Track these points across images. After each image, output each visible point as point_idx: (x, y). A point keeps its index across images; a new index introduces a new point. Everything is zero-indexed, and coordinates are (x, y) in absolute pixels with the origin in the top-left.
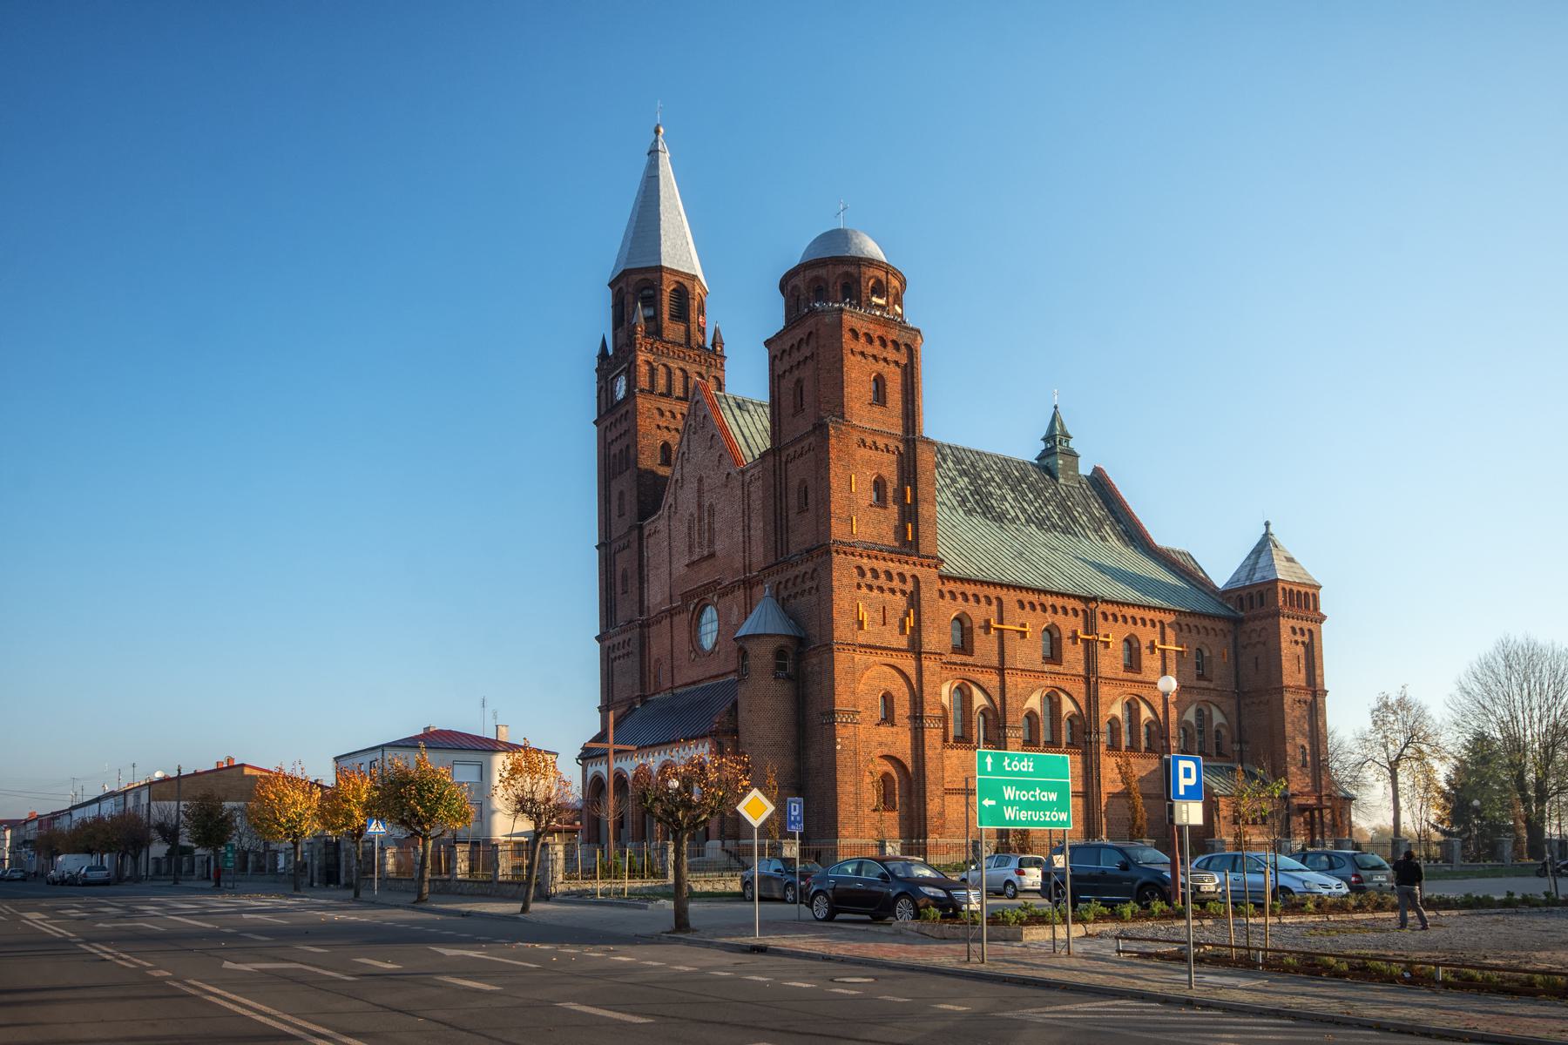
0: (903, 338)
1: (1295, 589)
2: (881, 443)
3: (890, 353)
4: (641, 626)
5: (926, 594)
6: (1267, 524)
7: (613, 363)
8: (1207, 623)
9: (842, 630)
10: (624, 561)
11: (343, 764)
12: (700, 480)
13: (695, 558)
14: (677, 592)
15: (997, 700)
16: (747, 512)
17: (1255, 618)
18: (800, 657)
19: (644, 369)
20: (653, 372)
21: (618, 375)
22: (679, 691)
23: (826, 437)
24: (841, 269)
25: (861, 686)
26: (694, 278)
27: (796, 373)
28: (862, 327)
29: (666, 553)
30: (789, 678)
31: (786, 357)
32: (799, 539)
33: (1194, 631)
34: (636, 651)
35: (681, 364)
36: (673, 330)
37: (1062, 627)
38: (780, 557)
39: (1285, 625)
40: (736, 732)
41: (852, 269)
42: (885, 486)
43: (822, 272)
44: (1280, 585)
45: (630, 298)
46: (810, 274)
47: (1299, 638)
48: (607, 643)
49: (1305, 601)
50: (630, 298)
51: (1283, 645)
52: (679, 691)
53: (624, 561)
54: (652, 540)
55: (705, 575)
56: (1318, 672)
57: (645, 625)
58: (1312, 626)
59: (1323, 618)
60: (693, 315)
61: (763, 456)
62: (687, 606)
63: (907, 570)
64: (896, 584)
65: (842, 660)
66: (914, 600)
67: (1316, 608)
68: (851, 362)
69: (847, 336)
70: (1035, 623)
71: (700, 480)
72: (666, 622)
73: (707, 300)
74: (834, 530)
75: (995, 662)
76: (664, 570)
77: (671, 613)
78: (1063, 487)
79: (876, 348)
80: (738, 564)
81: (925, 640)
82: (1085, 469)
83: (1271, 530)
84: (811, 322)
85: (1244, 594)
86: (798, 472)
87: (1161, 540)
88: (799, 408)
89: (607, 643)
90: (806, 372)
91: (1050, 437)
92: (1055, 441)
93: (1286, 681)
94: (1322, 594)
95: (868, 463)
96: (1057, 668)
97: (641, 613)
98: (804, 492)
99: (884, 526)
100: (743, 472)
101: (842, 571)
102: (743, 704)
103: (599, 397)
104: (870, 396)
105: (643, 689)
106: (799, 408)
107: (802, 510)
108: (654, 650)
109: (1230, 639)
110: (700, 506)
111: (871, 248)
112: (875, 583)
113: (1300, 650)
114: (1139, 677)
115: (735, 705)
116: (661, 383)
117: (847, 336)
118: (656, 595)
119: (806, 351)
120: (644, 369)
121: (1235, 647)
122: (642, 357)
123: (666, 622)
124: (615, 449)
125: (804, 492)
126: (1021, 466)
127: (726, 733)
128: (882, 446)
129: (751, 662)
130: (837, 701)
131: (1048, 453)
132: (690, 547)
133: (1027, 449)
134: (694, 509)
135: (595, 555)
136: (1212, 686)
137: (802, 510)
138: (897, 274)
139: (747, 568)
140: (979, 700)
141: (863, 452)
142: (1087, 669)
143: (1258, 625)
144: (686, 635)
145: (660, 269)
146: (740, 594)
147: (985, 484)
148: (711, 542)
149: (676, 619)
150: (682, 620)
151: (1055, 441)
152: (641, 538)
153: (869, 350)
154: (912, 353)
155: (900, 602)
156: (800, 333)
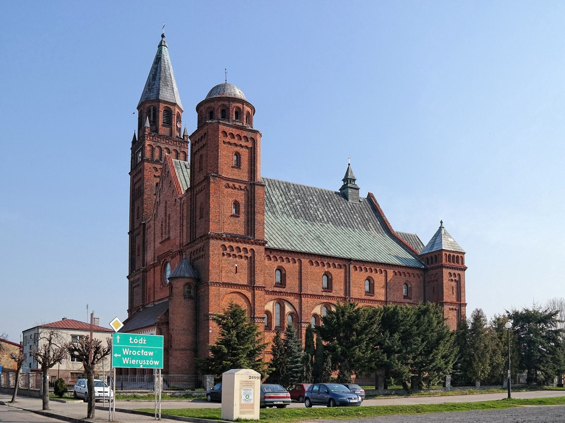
0: (250, 135)
1: (456, 255)
2: (237, 185)
3: (243, 143)
4: (143, 272)
5: (257, 258)
6: (441, 222)
7: (137, 145)
8: (409, 271)
9: (213, 277)
10: (139, 240)
11: (27, 334)
12: (166, 203)
13: (163, 239)
14: (156, 255)
15: (298, 309)
16: (182, 218)
17: (433, 268)
18: (197, 288)
19: (148, 148)
20: (153, 150)
21: (139, 151)
22: (156, 303)
23: (209, 183)
24: (221, 103)
25: (223, 302)
26: (175, 104)
27: (200, 152)
28: (229, 130)
29: (153, 237)
30: (191, 298)
31: (197, 144)
32: (199, 232)
33: (403, 275)
34: (141, 284)
35: (167, 146)
36: (163, 131)
37: (333, 273)
38: (193, 240)
39: (446, 272)
40: (168, 323)
41: (226, 103)
42: (239, 206)
43: (212, 104)
44: (444, 253)
45: (145, 114)
46: (207, 105)
47: (453, 278)
48: (132, 279)
49: (457, 260)
50: (145, 114)
51: (444, 281)
52: (156, 303)
53: (139, 240)
54: (149, 230)
55: (166, 248)
56: (462, 294)
57: (145, 271)
58: (460, 272)
59: (465, 269)
60: (174, 121)
61: (187, 191)
62: (160, 262)
63: (249, 247)
64: (242, 253)
65: (213, 290)
66: (252, 261)
67: (463, 263)
68: (222, 146)
69: (221, 134)
70: (320, 270)
71: (166, 203)
72: (152, 270)
73: (183, 116)
74: (211, 227)
75: (297, 290)
76: (152, 245)
77: (154, 266)
78: (352, 203)
79: (236, 141)
80: (178, 243)
81: (257, 280)
82: (363, 195)
83: (443, 225)
84: (206, 128)
85: (429, 256)
86: (200, 198)
87: (397, 227)
88: (201, 169)
89: (132, 279)
90: (203, 152)
91: (346, 179)
92: (348, 181)
93: (446, 299)
94: (466, 257)
95: (230, 195)
96: (329, 294)
97: (143, 266)
98: (202, 209)
99: (238, 225)
100: (181, 199)
101: (215, 246)
102: (170, 311)
103: (131, 161)
104: (234, 163)
105: (143, 302)
106: (201, 169)
107: (201, 217)
108: (149, 283)
109: (422, 278)
110: (166, 215)
111: (239, 93)
112: (232, 253)
113: (454, 284)
114: (373, 298)
115: (168, 311)
116: (157, 154)
117: (221, 134)
118: (149, 257)
119: (204, 142)
120: (148, 148)
121: (424, 283)
122: (147, 143)
123: (152, 270)
124: (137, 186)
125: (202, 209)
126: (329, 193)
127: (163, 324)
128: (237, 187)
129: (174, 291)
130: (210, 309)
131: (344, 188)
132: (162, 234)
133: (336, 186)
134: (163, 216)
135: (128, 236)
136: (411, 301)
137: (201, 217)
138: (248, 104)
139: (181, 244)
140: (288, 309)
141: (226, 190)
142: (346, 294)
143: (434, 272)
144: (159, 276)
145: (159, 101)
146: (178, 257)
147: (303, 202)
148: (169, 232)
149: (156, 268)
150: (158, 268)
151: (348, 181)
152: (144, 229)
153: (232, 141)
154: (254, 141)
155: (245, 262)
156: (202, 133)
